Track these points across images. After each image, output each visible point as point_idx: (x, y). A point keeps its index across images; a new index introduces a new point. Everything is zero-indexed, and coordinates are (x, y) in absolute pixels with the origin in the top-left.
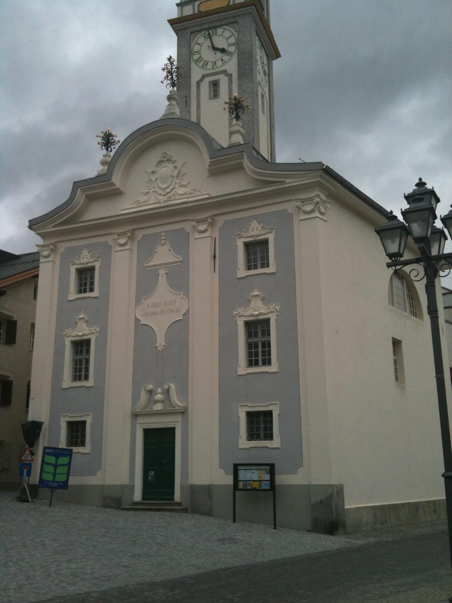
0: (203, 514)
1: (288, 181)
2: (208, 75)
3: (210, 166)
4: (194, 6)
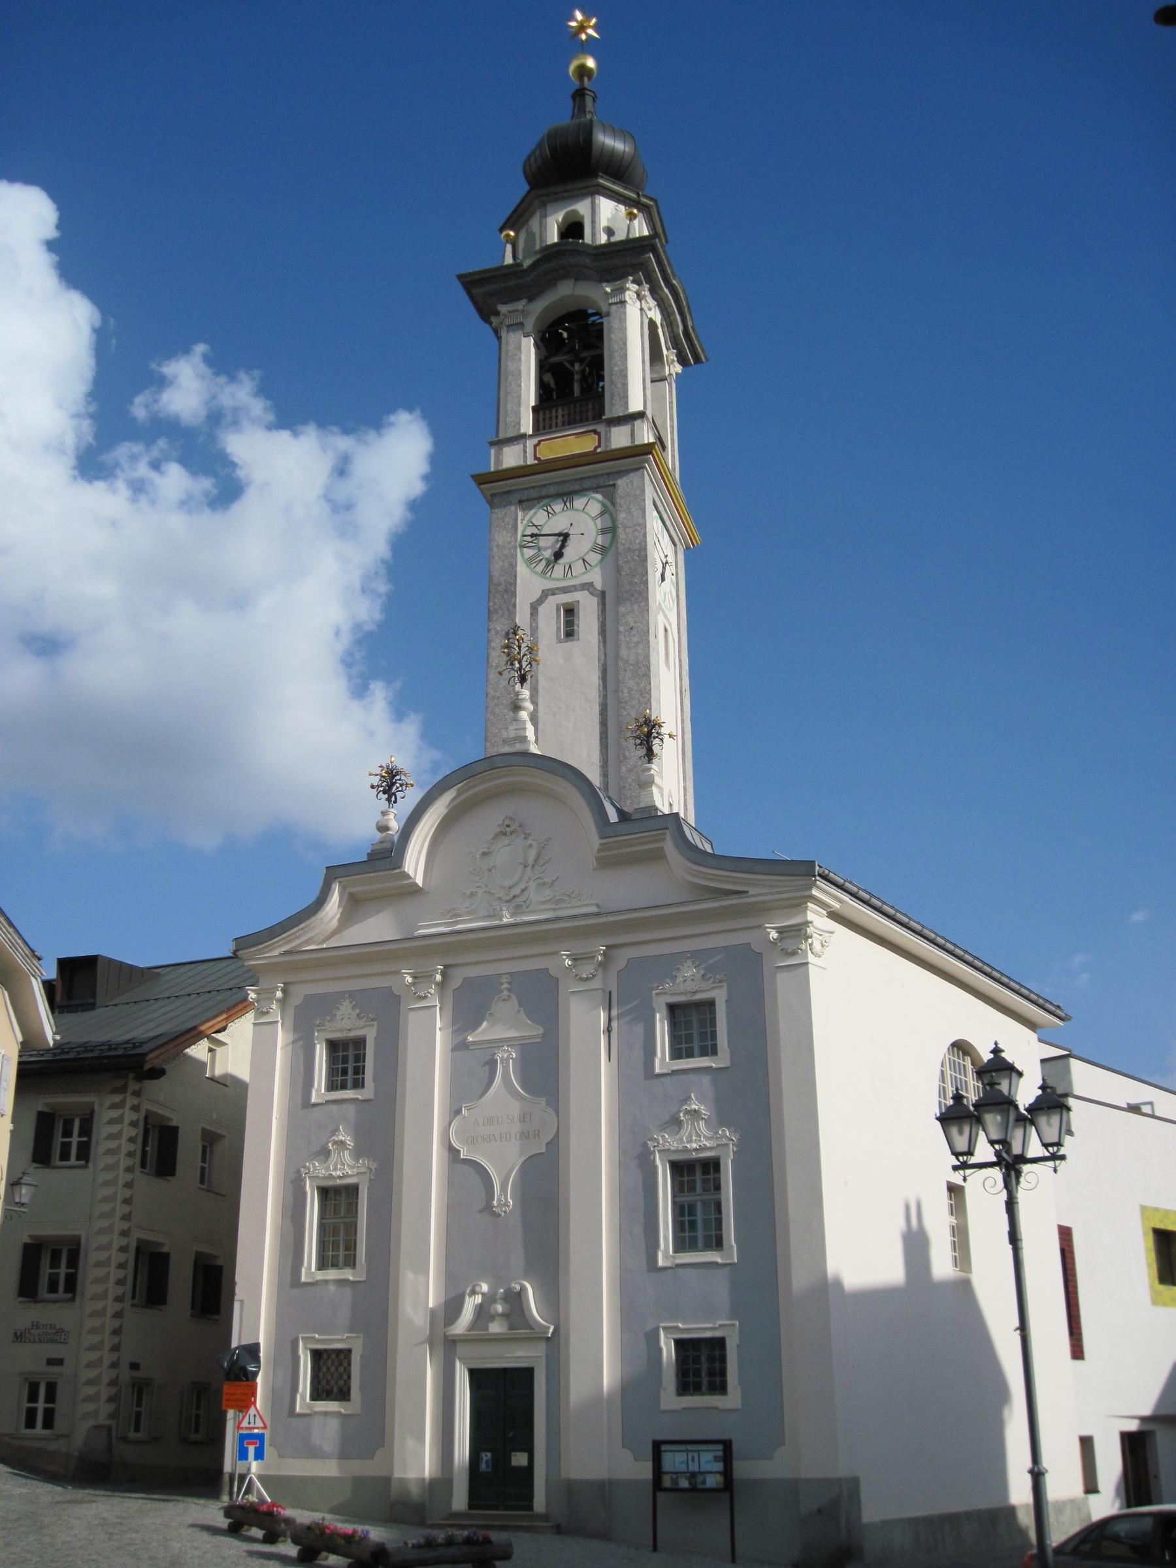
0: (592, 1536)
1: (752, 891)
2: (553, 592)
3: (599, 850)
4: (525, 446)
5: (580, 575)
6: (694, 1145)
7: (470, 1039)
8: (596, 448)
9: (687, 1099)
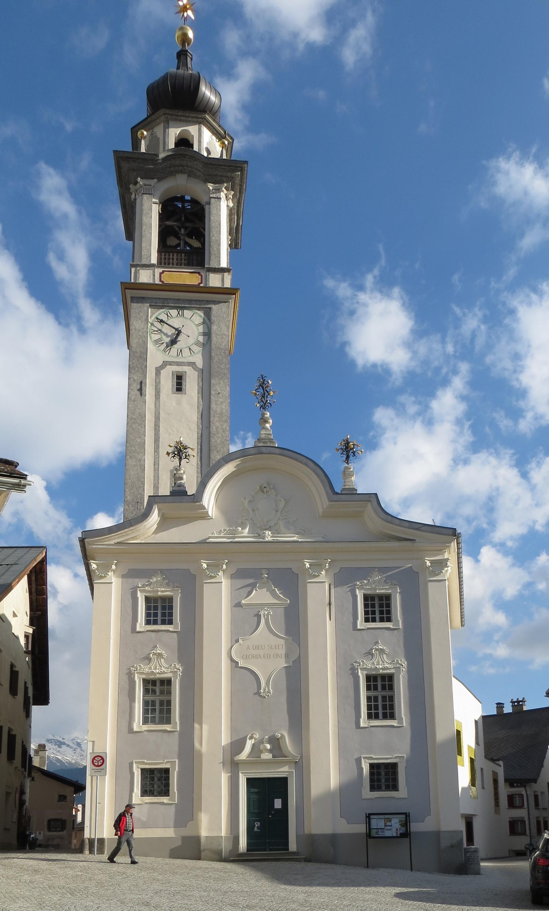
2: (171, 363)
4: (154, 272)
5: (187, 357)
6: (381, 667)
7: (243, 602)
8: (199, 284)
9: (377, 643)
